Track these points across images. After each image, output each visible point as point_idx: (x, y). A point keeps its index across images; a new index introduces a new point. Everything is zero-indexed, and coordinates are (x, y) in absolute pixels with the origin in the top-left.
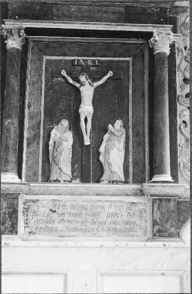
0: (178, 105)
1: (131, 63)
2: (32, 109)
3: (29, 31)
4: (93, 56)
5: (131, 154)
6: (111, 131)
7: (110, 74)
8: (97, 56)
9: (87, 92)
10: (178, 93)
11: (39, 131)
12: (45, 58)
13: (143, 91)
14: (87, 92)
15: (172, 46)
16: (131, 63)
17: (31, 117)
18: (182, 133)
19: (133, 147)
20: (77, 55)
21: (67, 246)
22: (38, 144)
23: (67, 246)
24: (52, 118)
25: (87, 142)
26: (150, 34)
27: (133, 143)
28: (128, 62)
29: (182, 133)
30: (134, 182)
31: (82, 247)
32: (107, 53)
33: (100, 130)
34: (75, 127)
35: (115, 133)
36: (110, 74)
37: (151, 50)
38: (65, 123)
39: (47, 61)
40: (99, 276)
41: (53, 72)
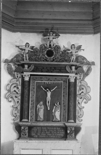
0: (77, 97)
1: (63, 83)
2: (32, 98)
3: (31, 75)
4: (51, 81)
5: (62, 112)
6: (79, 153)
7: (56, 87)
8: (52, 81)
9: (49, 94)
10: (77, 93)
11: (34, 105)
12: (36, 82)
13: (66, 93)
14: (49, 94)
15: (76, 80)
16: (63, 83)
17: (32, 101)
18: (78, 106)
19: (63, 110)
20: (46, 81)
21: (43, 142)
22: (34, 109)
23: (43, 142)
24: (38, 102)
25: (49, 109)
26: (68, 76)
27: (63, 109)
28: (62, 83)
29: (78, 106)
30: (63, 121)
31: (47, 142)
32: (55, 80)
33: (53, 105)
34: (45, 104)
35: (57, 106)
36: (56, 87)
37: (69, 80)
38: (41, 103)
39: (32, 77)
40: (21, 150)
41: (38, 87)
